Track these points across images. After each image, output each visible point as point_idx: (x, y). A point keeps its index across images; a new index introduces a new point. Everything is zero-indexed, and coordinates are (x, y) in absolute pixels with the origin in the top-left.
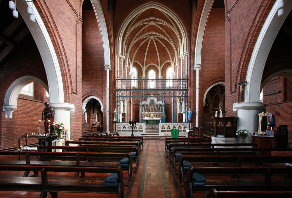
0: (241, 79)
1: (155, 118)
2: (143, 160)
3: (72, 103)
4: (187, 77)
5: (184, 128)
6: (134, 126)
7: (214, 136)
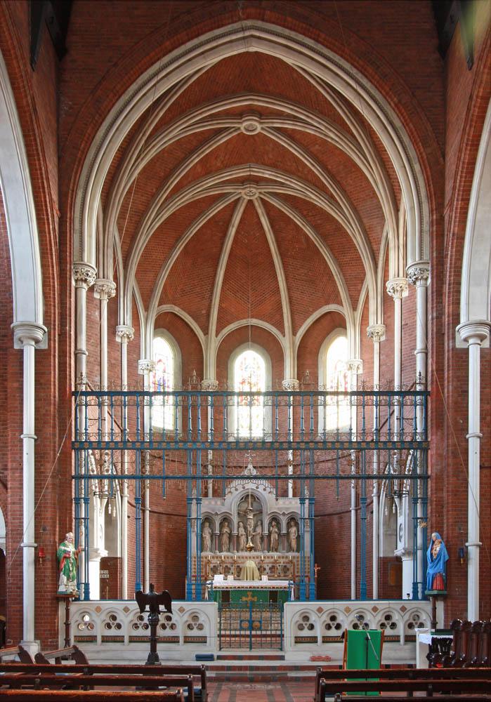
1: (265, 578)
4: (424, 381)
5: (411, 626)
6: (161, 617)
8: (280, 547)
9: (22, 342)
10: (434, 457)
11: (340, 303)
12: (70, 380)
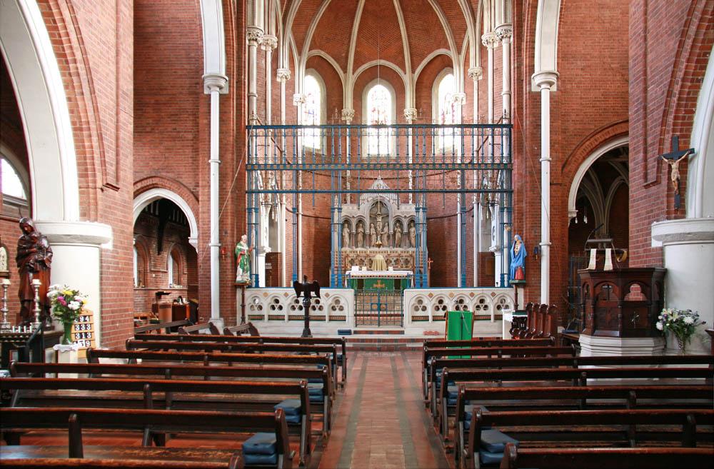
0: (675, 140)
1: (391, 268)
2: (345, 415)
3: (106, 220)
4: (508, 117)
5: (499, 308)
6: (313, 301)
7: (586, 333)
8: (403, 244)
9: (210, 89)
10: (517, 175)
11: (448, 48)
12: (245, 116)
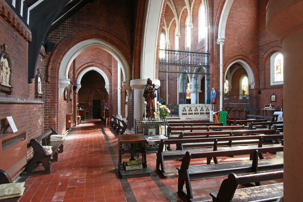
10: (211, 69)
